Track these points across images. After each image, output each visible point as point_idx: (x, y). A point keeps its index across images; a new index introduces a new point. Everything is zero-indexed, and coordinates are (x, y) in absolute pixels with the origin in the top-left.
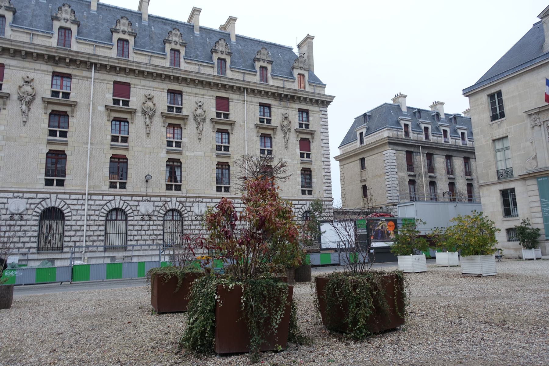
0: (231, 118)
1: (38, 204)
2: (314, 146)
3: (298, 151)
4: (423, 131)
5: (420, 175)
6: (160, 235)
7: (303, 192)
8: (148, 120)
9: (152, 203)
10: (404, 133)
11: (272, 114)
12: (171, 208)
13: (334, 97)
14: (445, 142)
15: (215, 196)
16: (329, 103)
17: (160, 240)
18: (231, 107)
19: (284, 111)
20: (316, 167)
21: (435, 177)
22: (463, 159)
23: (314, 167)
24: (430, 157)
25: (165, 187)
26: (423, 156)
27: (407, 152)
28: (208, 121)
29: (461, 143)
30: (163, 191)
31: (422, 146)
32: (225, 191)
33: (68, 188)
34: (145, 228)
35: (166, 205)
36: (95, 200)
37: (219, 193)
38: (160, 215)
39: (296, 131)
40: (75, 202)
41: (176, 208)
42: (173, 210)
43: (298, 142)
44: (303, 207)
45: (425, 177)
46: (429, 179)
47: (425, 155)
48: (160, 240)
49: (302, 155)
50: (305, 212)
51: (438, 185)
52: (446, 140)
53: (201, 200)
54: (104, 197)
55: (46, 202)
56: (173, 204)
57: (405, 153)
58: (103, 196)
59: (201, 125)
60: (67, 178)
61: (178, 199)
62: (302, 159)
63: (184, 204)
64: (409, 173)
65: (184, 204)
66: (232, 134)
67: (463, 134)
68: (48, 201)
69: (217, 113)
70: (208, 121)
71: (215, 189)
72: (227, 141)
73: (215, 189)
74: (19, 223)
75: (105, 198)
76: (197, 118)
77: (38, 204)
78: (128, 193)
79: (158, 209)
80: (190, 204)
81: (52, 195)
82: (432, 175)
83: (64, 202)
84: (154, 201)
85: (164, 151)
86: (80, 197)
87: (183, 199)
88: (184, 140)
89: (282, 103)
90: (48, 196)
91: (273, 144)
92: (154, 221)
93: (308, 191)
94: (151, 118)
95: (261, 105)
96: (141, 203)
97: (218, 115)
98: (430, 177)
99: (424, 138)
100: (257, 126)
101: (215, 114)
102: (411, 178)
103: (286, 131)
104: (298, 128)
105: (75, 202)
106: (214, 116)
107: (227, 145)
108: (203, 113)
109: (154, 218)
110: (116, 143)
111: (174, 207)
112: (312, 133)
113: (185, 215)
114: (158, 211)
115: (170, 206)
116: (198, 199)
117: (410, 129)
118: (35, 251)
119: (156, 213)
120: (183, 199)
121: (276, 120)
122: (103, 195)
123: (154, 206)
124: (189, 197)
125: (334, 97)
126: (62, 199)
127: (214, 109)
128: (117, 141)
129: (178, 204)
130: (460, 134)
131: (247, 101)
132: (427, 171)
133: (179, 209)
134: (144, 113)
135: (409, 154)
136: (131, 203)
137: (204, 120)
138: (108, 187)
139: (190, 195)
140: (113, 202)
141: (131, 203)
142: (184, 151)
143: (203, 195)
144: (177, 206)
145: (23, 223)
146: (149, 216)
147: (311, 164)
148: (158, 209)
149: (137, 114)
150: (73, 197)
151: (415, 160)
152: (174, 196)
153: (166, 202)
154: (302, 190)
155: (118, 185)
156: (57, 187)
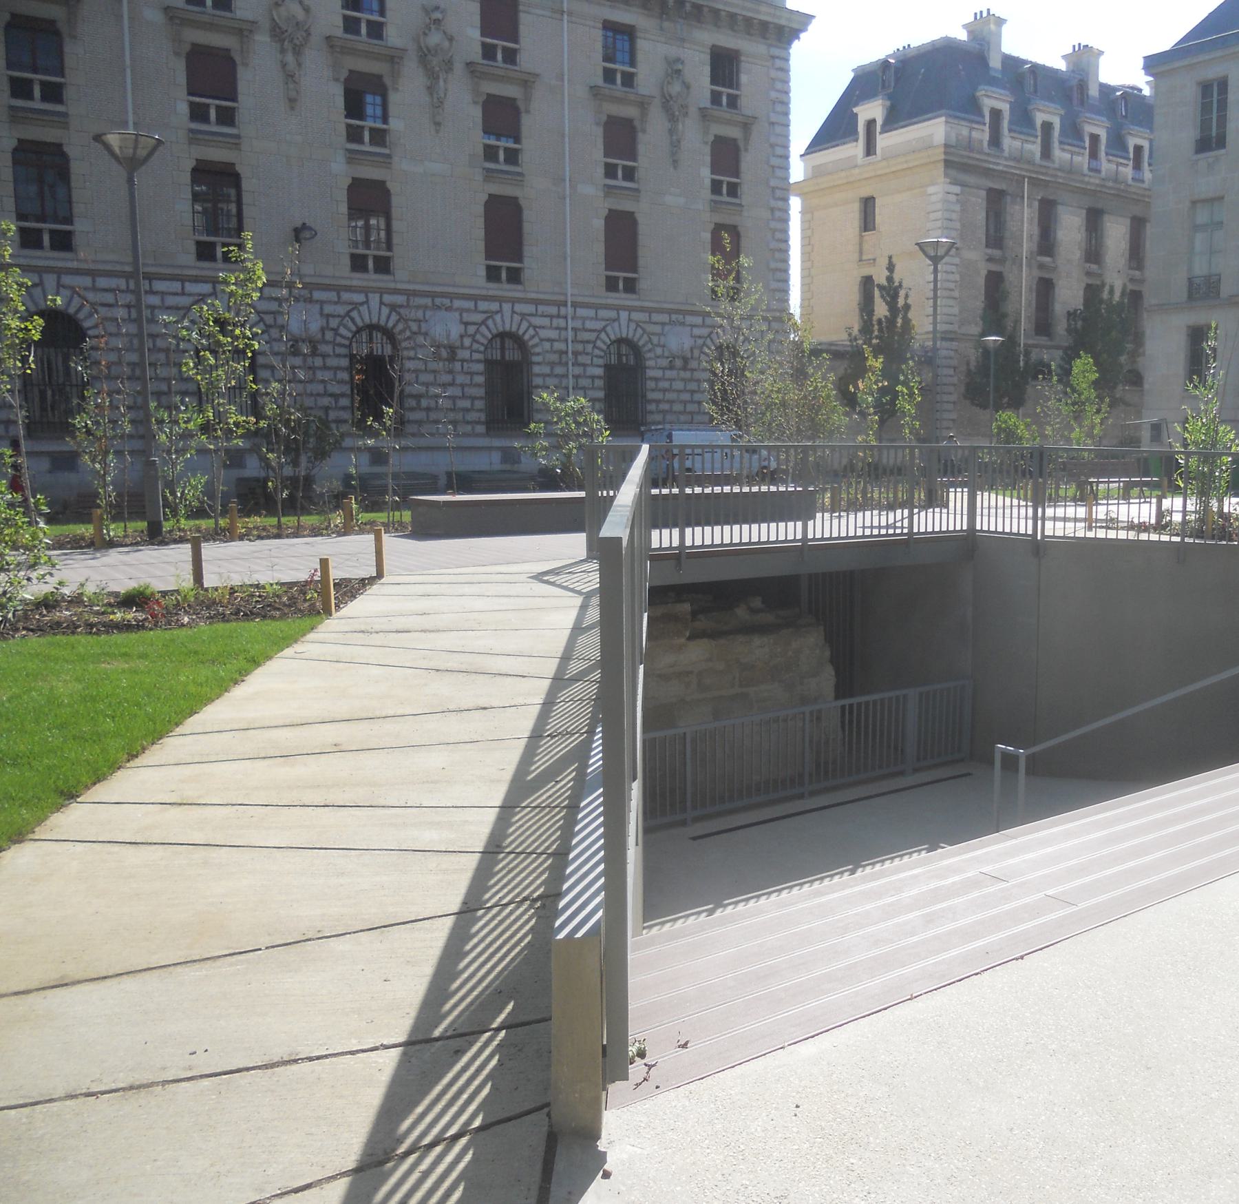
0: (526, 60)
1: (600, 331)
2: (749, 162)
3: (706, 174)
4: (1039, 133)
5: (1017, 260)
6: (343, 395)
7: (611, 284)
8: (290, 58)
9: (318, 306)
10: (986, 137)
11: (640, 56)
12: (367, 321)
13: (813, 17)
14: (1090, 169)
15: (484, 292)
16: (794, 34)
17: (344, 408)
18: (523, 30)
19: (673, 51)
20: (750, 219)
21: (1055, 268)
22: (1128, 221)
23: (643, 210)
24: (1094, 219)
25: (347, 261)
26: (1030, 206)
27: (990, 191)
28: (459, 67)
29: (1086, 166)
30: (342, 270)
31: (1030, 178)
32: (54, 247)
33: (85, 255)
34: (679, 385)
35: (355, 314)
36: (163, 293)
37: (491, 285)
38: (339, 339)
39: (704, 114)
40: (546, 322)
41: (382, 323)
42: (372, 328)
43: (708, 149)
44: (490, 322)
45: (1029, 266)
46: (1037, 273)
47: (1036, 204)
48: (344, 408)
49: (610, 171)
50: (613, 342)
51: (1057, 290)
52: (1094, 164)
53: (447, 302)
54: (480, 303)
55: (494, 320)
56: (374, 312)
57: (984, 193)
58: (183, 281)
59: (441, 83)
60: (80, 226)
61: (387, 298)
62: (194, 126)
63: (402, 311)
64: (989, 251)
65: (402, 311)
66: (397, 90)
67: (1138, 149)
68: (364, 309)
69: (484, 45)
70: (459, 67)
71: (482, 272)
72: (379, 112)
73: (483, 273)
74: (682, 374)
75: (190, 287)
76: (429, 57)
77: (600, 331)
78: (399, 286)
79: (471, 329)
80: (657, 329)
81: (45, 276)
82: (1047, 259)
83: (399, 314)
84: (322, 303)
85: (340, 158)
86: (553, 310)
87: (400, 299)
88: (395, 124)
89: (666, 24)
90: (613, 314)
91: (393, 110)
92: (324, 356)
93: (625, 279)
94: (298, 51)
95: (608, 26)
96: (667, 328)
97: (489, 52)
98: (1041, 266)
99: (1038, 155)
100: (595, 91)
101: (479, 49)
102: (994, 268)
103: (672, 109)
104: (708, 105)
105: (109, 298)
106: (476, 53)
107: (379, 125)
108: (446, 44)
109: (327, 349)
110: (204, 127)
111: (375, 321)
112: (527, 82)
113: (404, 344)
114: (335, 330)
115: (365, 316)
116: (440, 300)
117: (1005, 124)
118: (481, 429)
119: (329, 335)
120: (400, 299)
121: (648, 73)
122: (183, 279)
123: (321, 314)
124: (415, 293)
125: (813, 17)
126: (523, 316)
127: (476, 34)
128: (30, 96)
129: (385, 311)
130: (1131, 150)
131: (570, 14)
132: (1035, 248)
133: (390, 324)
134: (277, 33)
135: (996, 201)
136: (537, 321)
137: (449, 65)
138: (348, 268)
139: (418, 287)
140: (498, 318)
141: (537, 321)
142: (396, 159)
143: (450, 290)
144: (383, 316)
145: (688, 375)
146: (313, 344)
147: (237, 146)
148: (334, 323)
149: (258, 37)
150: (102, 282)
151: (1008, 218)
152: (625, 308)
153: (356, 306)
154: (608, 278)
155: (46, 239)
156: (56, 254)
